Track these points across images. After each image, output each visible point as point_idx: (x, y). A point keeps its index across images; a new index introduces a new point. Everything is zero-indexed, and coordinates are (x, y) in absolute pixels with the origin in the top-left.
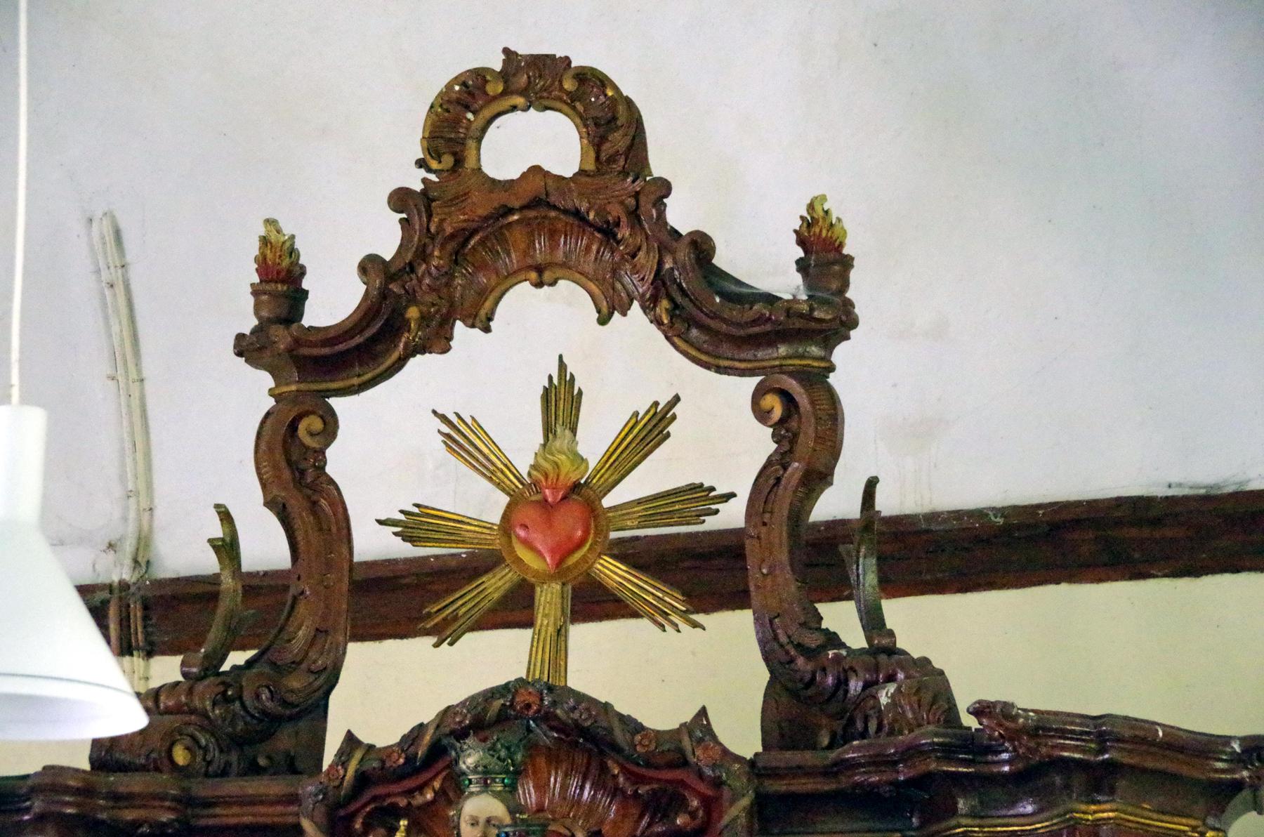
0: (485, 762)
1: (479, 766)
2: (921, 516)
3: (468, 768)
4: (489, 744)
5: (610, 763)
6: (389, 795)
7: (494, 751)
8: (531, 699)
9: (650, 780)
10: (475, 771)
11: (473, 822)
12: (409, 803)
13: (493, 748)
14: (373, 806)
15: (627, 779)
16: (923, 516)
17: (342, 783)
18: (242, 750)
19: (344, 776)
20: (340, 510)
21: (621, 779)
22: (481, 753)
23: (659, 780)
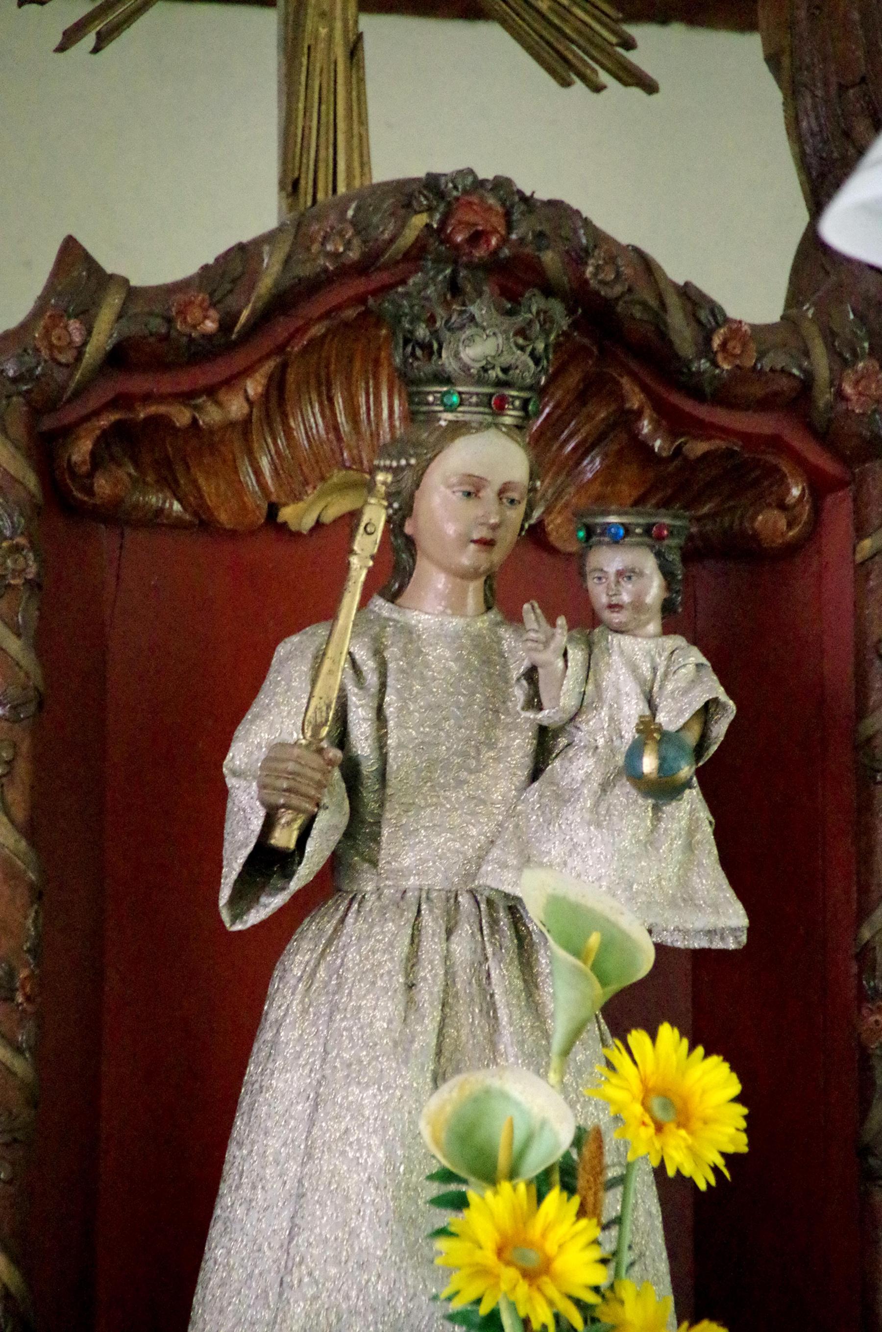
0: (506, 359)
1: (493, 368)
2: (553, 1077)
3: (466, 368)
4: (519, 320)
5: (626, 382)
6: (147, 398)
7: (526, 338)
9: (705, 430)
11: (468, 488)
12: (195, 421)
14: (114, 417)
15: (657, 426)
16: (545, 1077)
17: (79, 358)
18: (872, 432)
19: (85, 344)
20: (625, 78)
21: (646, 427)
22: (500, 341)
23: (725, 432)
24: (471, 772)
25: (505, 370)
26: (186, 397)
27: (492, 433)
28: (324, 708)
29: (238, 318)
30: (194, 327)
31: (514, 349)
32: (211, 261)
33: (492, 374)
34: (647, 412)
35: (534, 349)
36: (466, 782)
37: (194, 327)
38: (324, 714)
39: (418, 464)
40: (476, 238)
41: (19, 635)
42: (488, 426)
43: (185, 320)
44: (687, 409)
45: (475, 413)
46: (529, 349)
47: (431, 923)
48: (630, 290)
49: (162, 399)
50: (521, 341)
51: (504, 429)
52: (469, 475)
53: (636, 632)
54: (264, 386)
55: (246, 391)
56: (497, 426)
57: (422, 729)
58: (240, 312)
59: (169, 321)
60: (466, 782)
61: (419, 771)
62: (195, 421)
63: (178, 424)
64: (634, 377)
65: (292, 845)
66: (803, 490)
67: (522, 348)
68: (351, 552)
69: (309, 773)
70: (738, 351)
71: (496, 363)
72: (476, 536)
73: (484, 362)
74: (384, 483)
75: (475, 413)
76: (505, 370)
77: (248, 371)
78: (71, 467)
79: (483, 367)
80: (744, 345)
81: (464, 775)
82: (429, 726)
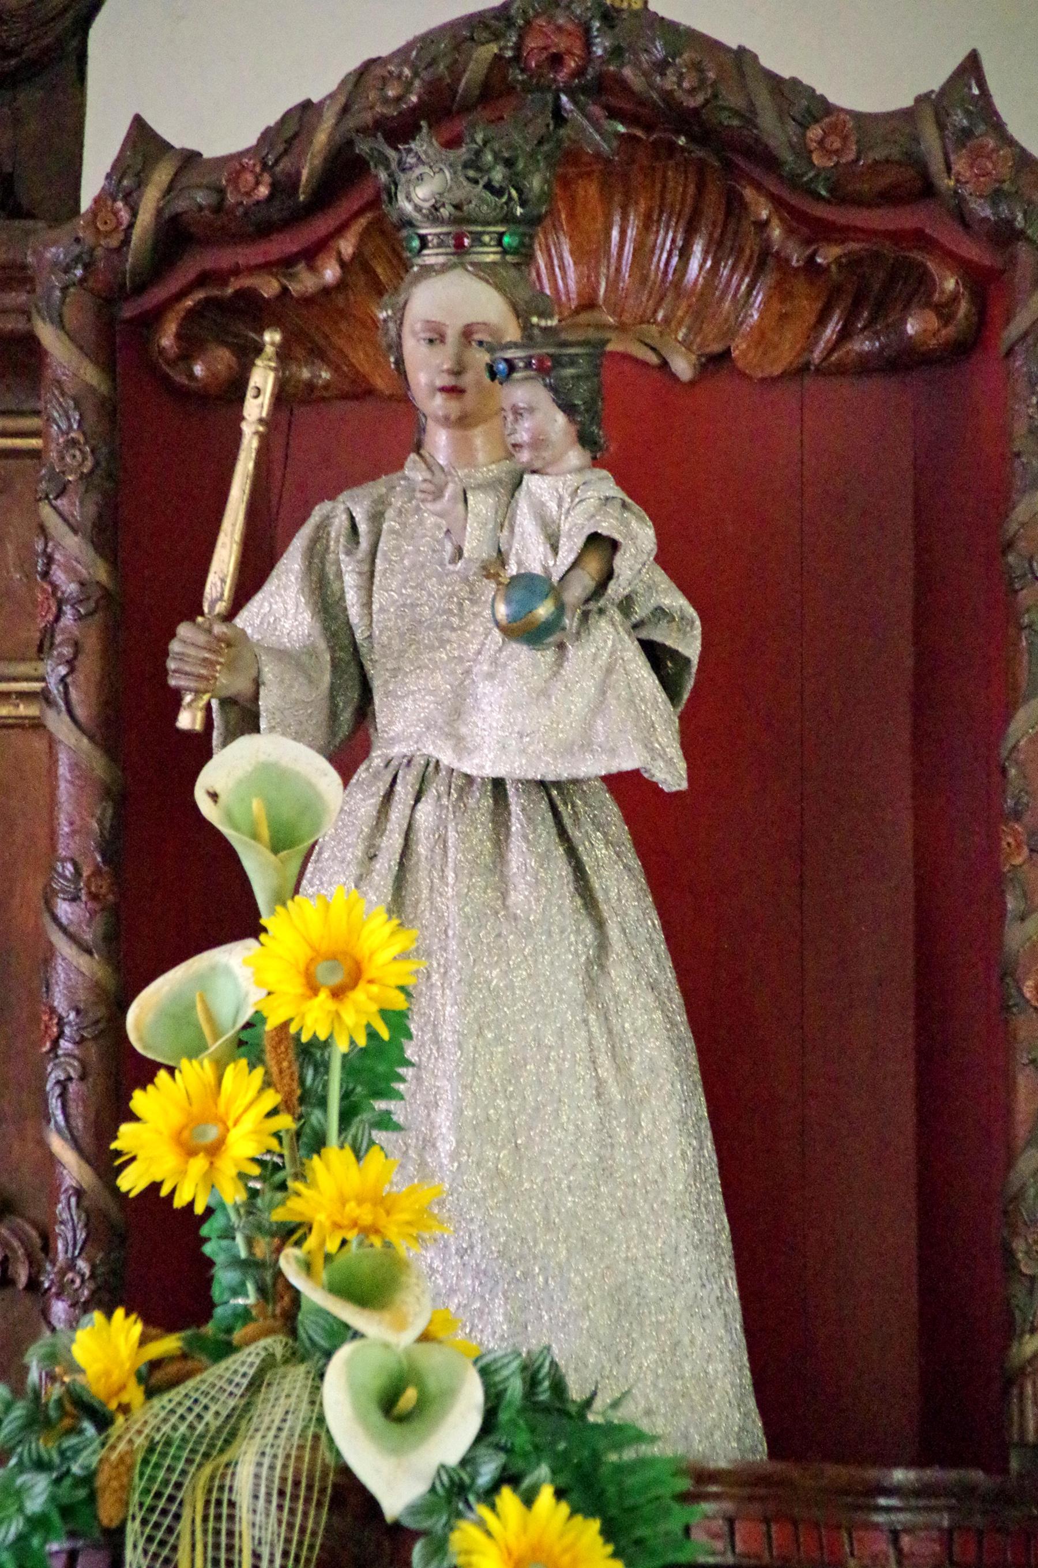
0: (459, 195)
7: (479, 169)
8: (561, 43)
10: (433, 215)
12: (285, 290)
13: (473, 163)
14: (200, 295)
15: (790, 232)
17: (126, 241)
19: (131, 226)
24: (453, 630)
25: (458, 207)
26: (267, 267)
27: (458, 272)
28: (219, 583)
29: (299, 180)
30: (248, 194)
31: (465, 183)
32: (818, 92)
33: (445, 212)
34: (775, 222)
35: (490, 181)
36: (449, 641)
37: (248, 194)
38: (219, 589)
39: (394, 314)
40: (556, 60)
41: (75, 532)
42: (454, 266)
43: (237, 188)
44: (818, 214)
45: (437, 254)
46: (482, 183)
47: (404, 792)
48: (715, 96)
49: (253, 270)
50: (471, 173)
51: (470, 268)
52: (428, 322)
53: (549, 470)
54: (354, 246)
55: (339, 253)
56: (463, 265)
57: (404, 591)
58: (299, 173)
59: (221, 191)
60: (449, 641)
61: (402, 636)
62: (285, 290)
63: (266, 295)
64: (759, 187)
65: (198, 727)
66: (957, 283)
67: (476, 182)
68: (243, 418)
69: (192, 651)
70: (838, 145)
71: (444, 200)
72: (439, 383)
73: (433, 201)
74: (273, 344)
75: (437, 254)
76: (458, 207)
77: (340, 230)
78: (162, 351)
79: (433, 206)
80: (845, 139)
81: (447, 634)
82: (411, 587)
